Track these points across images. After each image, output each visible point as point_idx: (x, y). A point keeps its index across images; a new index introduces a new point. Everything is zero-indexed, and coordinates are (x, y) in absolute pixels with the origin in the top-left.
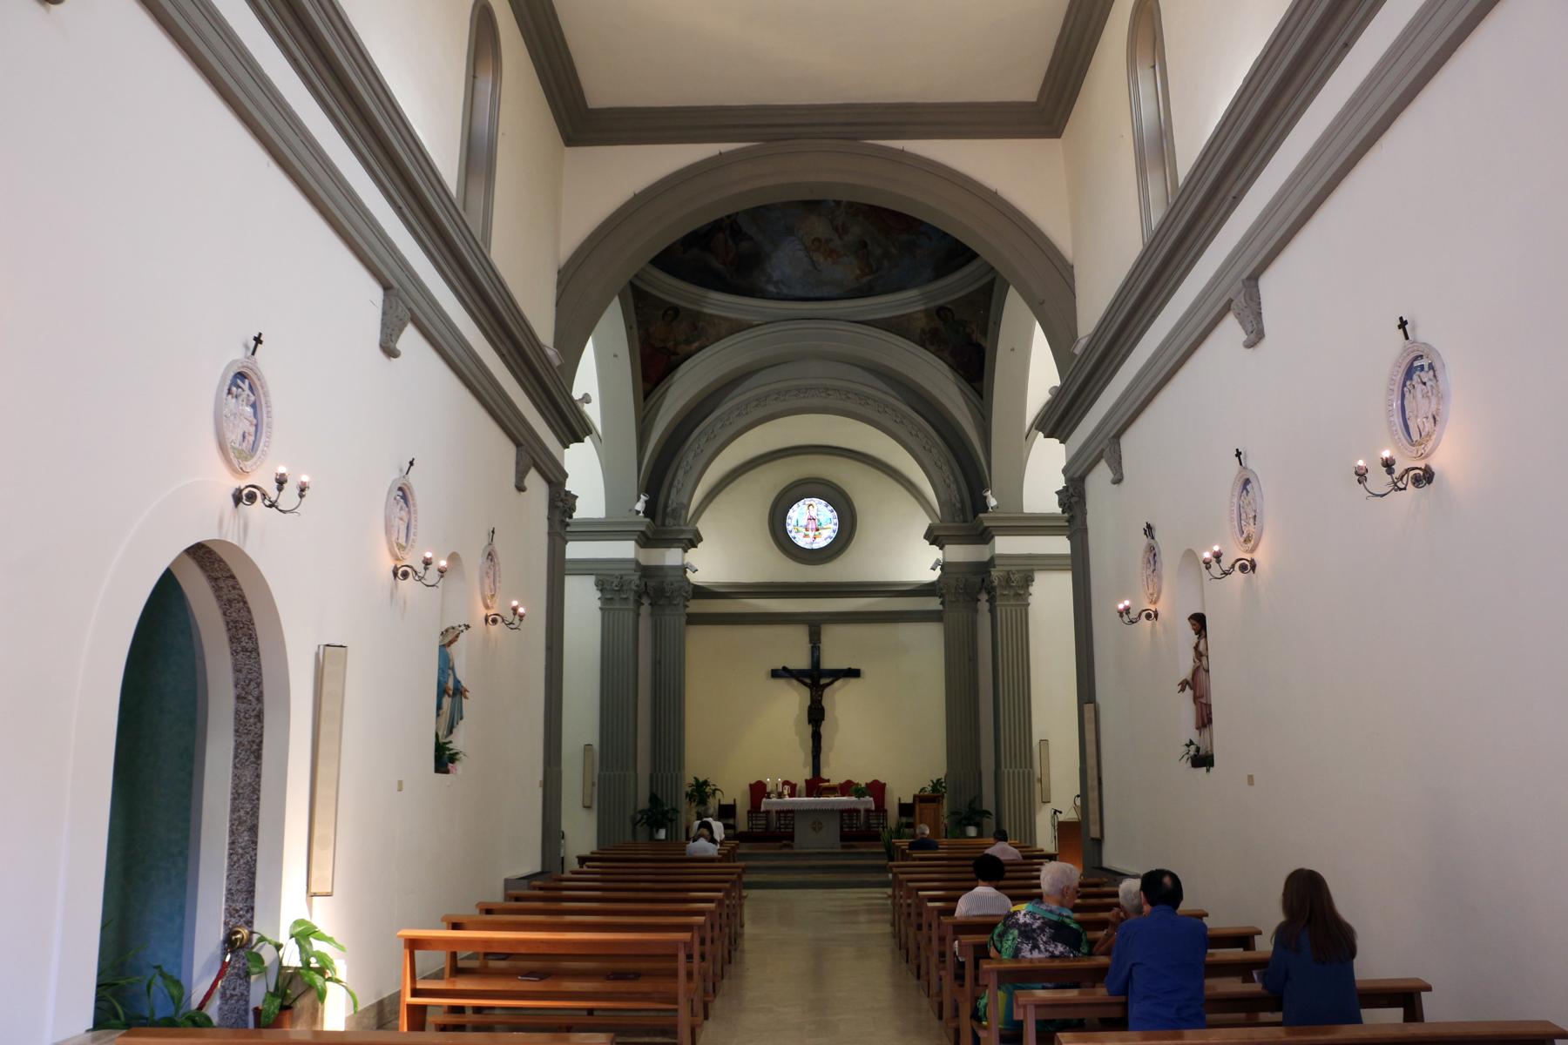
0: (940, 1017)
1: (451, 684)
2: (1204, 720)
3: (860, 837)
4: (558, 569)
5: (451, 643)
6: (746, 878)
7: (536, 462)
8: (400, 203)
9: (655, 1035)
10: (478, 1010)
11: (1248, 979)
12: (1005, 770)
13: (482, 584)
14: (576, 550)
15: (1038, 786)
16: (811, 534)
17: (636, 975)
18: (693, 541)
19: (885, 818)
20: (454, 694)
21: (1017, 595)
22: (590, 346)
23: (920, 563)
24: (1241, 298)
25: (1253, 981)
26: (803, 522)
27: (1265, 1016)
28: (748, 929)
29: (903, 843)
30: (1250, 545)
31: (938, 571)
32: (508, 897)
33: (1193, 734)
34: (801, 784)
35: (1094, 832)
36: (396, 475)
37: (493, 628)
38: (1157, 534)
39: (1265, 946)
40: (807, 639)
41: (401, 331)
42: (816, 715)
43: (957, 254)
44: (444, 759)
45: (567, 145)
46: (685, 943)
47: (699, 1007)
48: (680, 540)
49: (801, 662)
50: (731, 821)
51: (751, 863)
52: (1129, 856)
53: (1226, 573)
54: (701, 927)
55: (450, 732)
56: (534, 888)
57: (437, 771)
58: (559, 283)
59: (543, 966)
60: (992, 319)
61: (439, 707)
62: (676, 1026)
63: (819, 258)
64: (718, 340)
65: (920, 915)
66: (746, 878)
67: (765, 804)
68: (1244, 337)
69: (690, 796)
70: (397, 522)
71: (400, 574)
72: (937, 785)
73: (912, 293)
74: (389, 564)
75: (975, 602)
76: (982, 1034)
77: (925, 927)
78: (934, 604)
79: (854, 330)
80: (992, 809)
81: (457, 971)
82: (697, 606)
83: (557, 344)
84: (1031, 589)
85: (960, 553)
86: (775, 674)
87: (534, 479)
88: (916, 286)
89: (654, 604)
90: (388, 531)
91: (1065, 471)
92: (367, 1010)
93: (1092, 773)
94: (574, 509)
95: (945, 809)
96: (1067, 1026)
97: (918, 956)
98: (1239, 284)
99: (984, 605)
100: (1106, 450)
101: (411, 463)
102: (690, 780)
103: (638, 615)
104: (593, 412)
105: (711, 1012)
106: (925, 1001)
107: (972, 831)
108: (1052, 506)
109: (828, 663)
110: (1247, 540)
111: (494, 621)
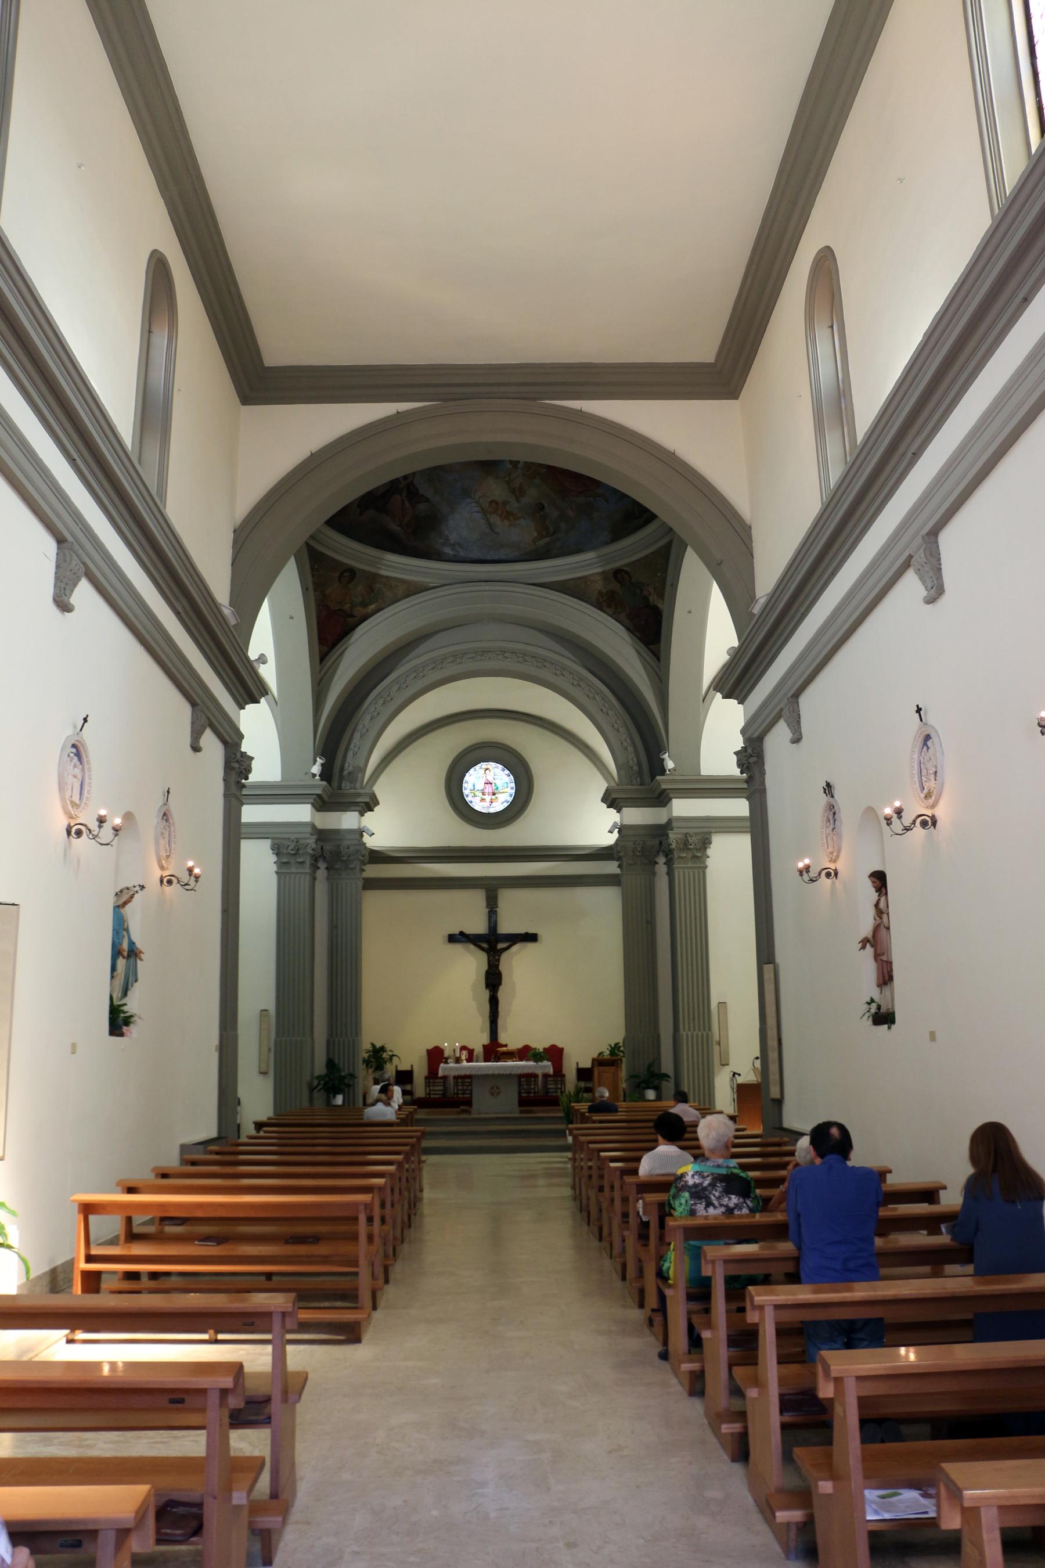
0: (624, 1278)
1: (125, 945)
2: (886, 978)
3: (540, 1100)
4: (234, 833)
5: (125, 903)
6: (425, 1144)
7: (211, 722)
8: (75, 456)
9: (335, 1300)
10: (154, 1276)
11: (934, 1231)
12: (683, 1033)
13: (157, 844)
14: (251, 814)
15: (716, 1048)
16: (488, 798)
17: (316, 1239)
18: (369, 805)
19: (563, 1083)
20: (129, 956)
21: (695, 857)
22: (266, 600)
23: (597, 826)
24: (921, 554)
25: (941, 1233)
26: (480, 786)
27: (949, 1269)
28: (427, 1194)
29: (583, 1107)
30: (931, 801)
31: (616, 835)
32: (184, 1162)
33: (874, 992)
34: (479, 1050)
35: (774, 1093)
36: (69, 732)
37: (168, 889)
38: (837, 793)
39: (952, 1199)
40: (484, 904)
41: (75, 585)
42: (493, 980)
43: (634, 516)
44: (118, 1022)
45: (246, 399)
46: (366, 1205)
47: (379, 1271)
48: (357, 804)
49: (478, 926)
50: (408, 1087)
51: (429, 1129)
52: (800, 1116)
53: (907, 829)
54: (380, 1189)
55: (125, 994)
56: (211, 1153)
57: (112, 1033)
58: (235, 542)
59: (221, 1230)
60: (668, 583)
61: (113, 968)
62: (357, 1289)
63: (495, 519)
64: (394, 602)
65: (601, 1177)
66: (425, 1144)
67: (443, 1069)
68: (924, 593)
69: (367, 1063)
70: (70, 779)
71: (73, 832)
72: (614, 1049)
73: (590, 556)
74: (63, 822)
75: (652, 864)
76: (669, 1292)
77: (607, 1189)
78: (611, 867)
79: (533, 593)
80: (671, 1073)
81: (132, 1236)
82: (373, 871)
83: (232, 603)
84: (709, 852)
85: (637, 816)
86: (452, 939)
87: (209, 740)
88: (594, 548)
89: (331, 868)
90: (61, 788)
91: (743, 732)
92: (39, 1278)
93: (772, 1033)
94: (249, 770)
95: (623, 1073)
96: (753, 1281)
97: (600, 1219)
98: (919, 540)
99: (661, 868)
100: (786, 708)
101: (85, 720)
102: (366, 1045)
103: (314, 879)
104: (268, 673)
105: (392, 1276)
106: (607, 1262)
107: (651, 1094)
108: (731, 768)
109: (505, 927)
110: (928, 796)
111: (170, 882)
